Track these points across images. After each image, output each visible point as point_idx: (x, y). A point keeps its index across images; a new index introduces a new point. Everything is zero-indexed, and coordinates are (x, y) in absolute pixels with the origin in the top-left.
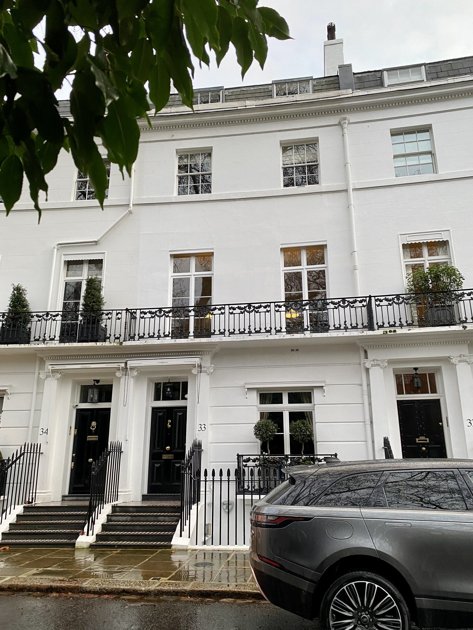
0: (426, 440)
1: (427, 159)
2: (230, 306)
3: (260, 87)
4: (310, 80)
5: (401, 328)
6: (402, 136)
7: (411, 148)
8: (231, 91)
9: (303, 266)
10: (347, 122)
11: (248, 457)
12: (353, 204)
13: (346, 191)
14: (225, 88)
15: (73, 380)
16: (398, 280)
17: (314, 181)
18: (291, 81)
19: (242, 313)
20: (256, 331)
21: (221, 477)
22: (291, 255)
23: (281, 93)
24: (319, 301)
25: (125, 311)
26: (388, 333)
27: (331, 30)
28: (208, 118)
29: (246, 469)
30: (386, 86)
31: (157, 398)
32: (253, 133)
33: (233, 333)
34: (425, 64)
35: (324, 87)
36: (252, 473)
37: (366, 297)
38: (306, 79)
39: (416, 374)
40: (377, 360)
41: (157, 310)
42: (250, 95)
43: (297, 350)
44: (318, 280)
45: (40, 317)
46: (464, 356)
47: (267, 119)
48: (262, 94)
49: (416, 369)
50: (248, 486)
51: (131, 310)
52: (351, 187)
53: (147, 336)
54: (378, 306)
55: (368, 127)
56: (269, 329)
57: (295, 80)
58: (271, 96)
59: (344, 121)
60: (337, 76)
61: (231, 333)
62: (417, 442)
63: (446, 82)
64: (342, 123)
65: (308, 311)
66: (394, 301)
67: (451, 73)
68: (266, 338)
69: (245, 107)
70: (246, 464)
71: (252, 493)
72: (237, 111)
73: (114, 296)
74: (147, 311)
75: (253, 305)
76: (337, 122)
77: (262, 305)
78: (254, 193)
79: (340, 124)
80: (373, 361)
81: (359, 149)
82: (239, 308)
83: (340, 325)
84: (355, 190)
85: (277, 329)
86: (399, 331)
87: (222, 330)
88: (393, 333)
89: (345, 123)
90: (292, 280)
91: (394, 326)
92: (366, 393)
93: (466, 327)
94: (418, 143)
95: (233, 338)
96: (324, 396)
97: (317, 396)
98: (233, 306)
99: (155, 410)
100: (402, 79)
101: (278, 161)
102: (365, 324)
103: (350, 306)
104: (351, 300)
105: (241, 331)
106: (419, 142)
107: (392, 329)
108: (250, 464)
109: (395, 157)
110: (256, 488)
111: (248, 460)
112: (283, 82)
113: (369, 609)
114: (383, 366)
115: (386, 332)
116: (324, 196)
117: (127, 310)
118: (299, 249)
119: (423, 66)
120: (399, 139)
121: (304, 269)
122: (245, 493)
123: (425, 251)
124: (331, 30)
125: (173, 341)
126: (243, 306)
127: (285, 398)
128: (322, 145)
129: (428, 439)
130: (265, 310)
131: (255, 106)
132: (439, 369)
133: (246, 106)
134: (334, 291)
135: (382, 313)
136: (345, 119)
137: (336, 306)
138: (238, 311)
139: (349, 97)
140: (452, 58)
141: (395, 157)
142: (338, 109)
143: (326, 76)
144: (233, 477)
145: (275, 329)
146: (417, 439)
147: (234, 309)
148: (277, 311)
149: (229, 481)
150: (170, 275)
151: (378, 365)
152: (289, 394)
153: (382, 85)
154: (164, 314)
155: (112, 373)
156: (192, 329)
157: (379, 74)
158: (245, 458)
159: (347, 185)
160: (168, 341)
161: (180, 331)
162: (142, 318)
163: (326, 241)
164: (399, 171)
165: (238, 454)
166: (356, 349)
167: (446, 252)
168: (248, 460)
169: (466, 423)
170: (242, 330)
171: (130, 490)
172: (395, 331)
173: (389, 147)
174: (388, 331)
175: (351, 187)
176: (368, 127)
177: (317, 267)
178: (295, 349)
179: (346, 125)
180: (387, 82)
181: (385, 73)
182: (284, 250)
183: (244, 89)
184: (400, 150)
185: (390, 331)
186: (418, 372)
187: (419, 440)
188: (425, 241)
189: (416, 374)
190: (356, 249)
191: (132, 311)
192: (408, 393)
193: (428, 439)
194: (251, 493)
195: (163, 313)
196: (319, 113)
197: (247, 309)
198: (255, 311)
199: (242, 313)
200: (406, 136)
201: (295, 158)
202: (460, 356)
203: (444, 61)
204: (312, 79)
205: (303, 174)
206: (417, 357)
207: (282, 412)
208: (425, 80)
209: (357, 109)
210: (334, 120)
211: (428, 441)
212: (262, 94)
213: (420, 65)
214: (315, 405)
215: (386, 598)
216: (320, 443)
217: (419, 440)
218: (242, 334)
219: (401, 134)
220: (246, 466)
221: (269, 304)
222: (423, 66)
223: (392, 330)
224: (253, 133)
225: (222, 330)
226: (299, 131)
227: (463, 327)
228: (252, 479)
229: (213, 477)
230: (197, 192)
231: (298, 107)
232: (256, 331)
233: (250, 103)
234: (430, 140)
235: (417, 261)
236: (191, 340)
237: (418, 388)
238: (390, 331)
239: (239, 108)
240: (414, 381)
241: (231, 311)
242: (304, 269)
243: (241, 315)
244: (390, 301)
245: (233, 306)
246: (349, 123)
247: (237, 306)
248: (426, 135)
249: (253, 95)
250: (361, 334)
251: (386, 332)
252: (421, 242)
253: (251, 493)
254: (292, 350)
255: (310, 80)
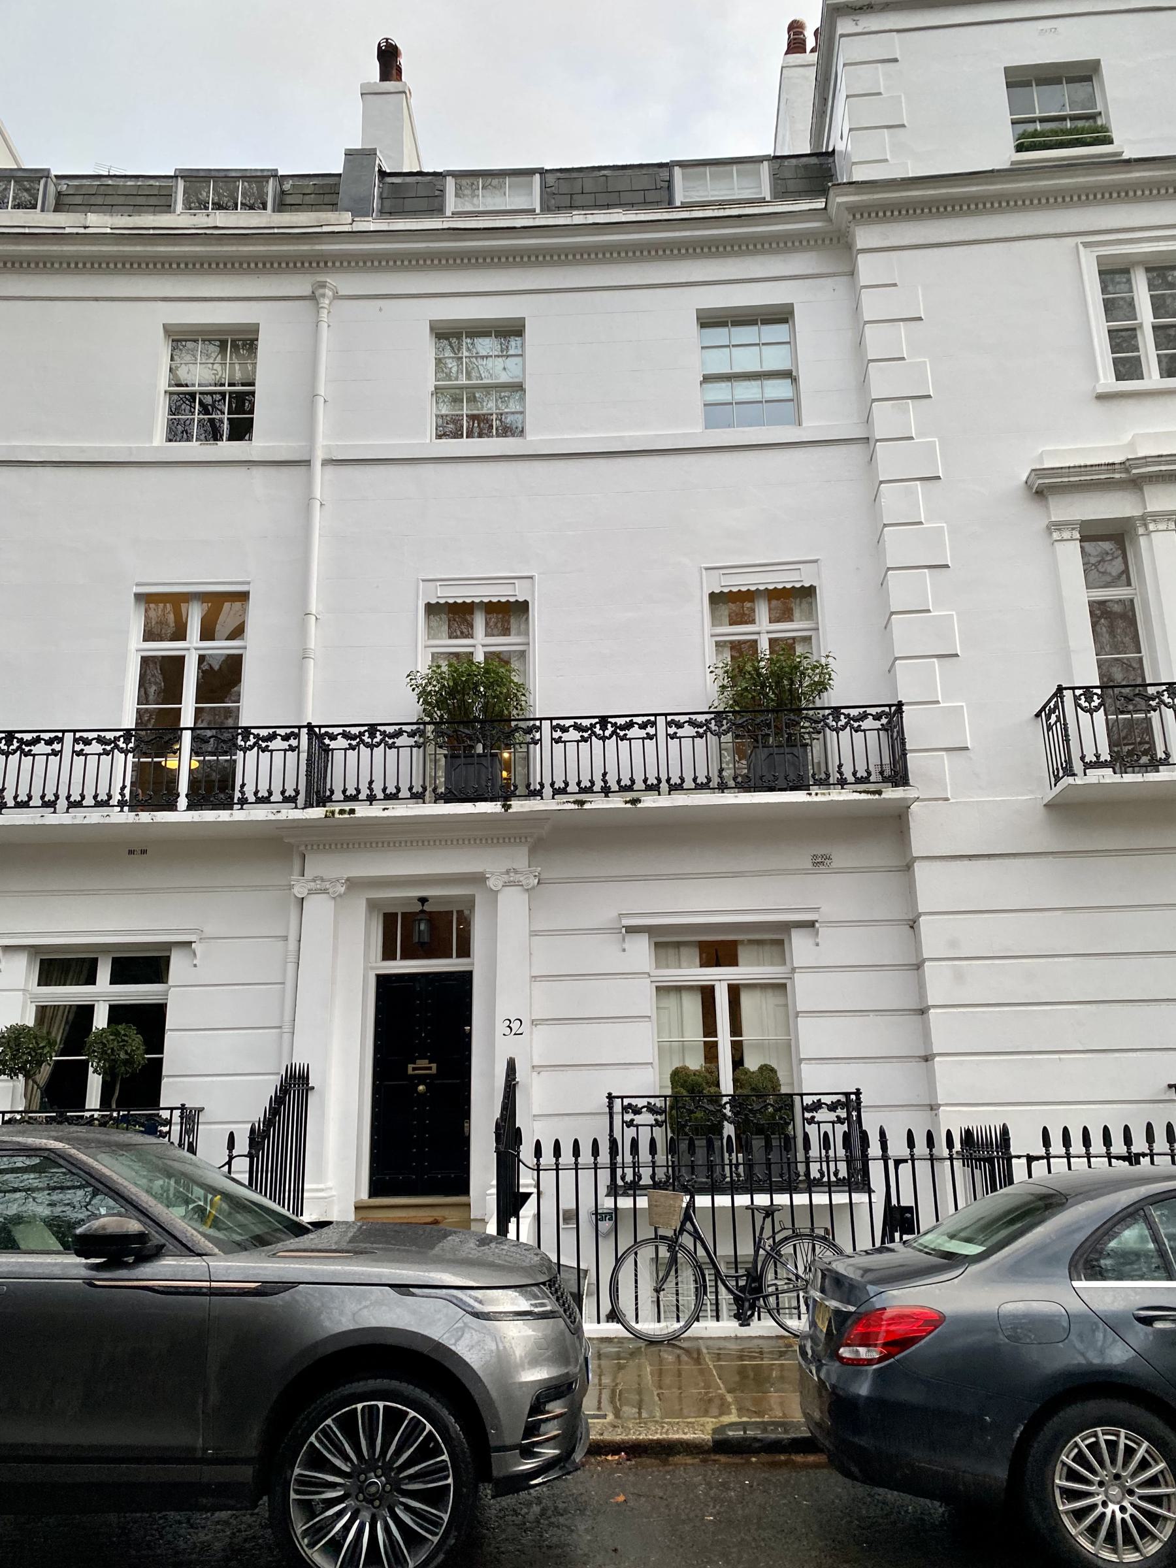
0: (430, 1068)
1: (779, 389)
2: (78, 735)
3: (152, 182)
4: (269, 177)
5: (607, 796)
6: (725, 330)
7: (746, 361)
8: (76, 182)
9: (190, 642)
10: (329, 293)
11: (815, 1098)
12: (318, 496)
13: (307, 463)
14: (53, 173)
15: (367, 899)
16: (691, 677)
17: (242, 430)
18: (222, 174)
19: (354, 749)
20: (647, 786)
21: (557, 1160)
22: (164, 612)
23: (195, 203)
24: (223, 736)
25: (305, 730)
26: (337, 816)
27: (388, 57)
28: (26, 248)
29: (812, 1130)
30: (448, 214)
31: (388, 954)
32: (96, 299)
33: (78, 804)
34: (542, 172)
35: (308, 199)
36: (826, 1142)
37: (299, 727)
38: (259, 174)
39: (422, 911)
40: (322, 880)
41: (118, 734)
42: (121, 200)
43: (144, 852)
44: (223, 679)
45: (353, 738)
46: (516, 871)
47: (135, 266)
48: (153, 201)
49: (423, 900)
50: (821, 1171)
51: (320, 727)
52: (319, 455)
53: (88, 801)
54: (78, 755)
55: (381, 310)
56: (293, 794)
57: (234, 174)
58: (168, 208)
59: (321, 291)
60: (340, 175)
61: (73, 805)
62: (410, 1072)
63: (568, 221)
64: (317, 294)
65: (130, 755)
66: (708, 728)
67: (602, 199)
68: (38, 821)
69: (82, 231)
70: (813, 1117)
71: (830, 1188)
72: (58, 237)
73: (553, 686)
74: (336, 731)
75: (613, 720)
76: (307, 291)
77: (635, 720)
78: (82, 450)
79: (313, 297)
80: (314, 880)
81: (354, 360)
82: (577, 727)
83: (592, 782)
84: (326, 462)
85: (556, 786)
86: (363, 811)
87: (652, 781)
88: (346, 816)
89: (323, 295)
90: (161, 676)
91: (354, 798)
92: (292, 958)
93: (510, 806)
94: (749, 351)
95: (77, 817)
96: (195, 966)
97: (178, 965)
98: (676, 718)
99: (385, 983)
100: (489, 200)
101: (151, 375)
102: (887, 773)
103: (260, 747)
104: (854, 712)
105: (348, 793)
106: (733, 349)
107: (347, 807)
108: (822, 1115)
109: (707, 379)
110: (840, 1176)
111: (817, 1106)
112: (202, 174)
113: (392, 1469)
114: (528, 884)
115: (333, 812)
116: (257, 472)
117: (310, 727)
118: (188, 597)
119: (766, 163)
120: (719, 335)
121: (192, 648)
122: (638, 1192)
123: (479, 622)
124: (388, 57)
125: (127, 817)
126: (586, 723)
127: (104, 972)
128: (1011, 144)
129: (434, 1066)
130: (643, 733)
131: (109, 231)
132: (471, 902)
133: (85, 227)
134: (255, 706)
135: (348, 768)
136: (323, 285)
137: (586, 735)
138: (574, 735)
139: (333, 232)
140: (558, 167)
141: (707, 379)
142: (307, 259)
143: (778, 154)
144: (604, 1157)
145: (68, 797)
146: (410, 1066)
147: (565, 730)
148: (673, 736)
149: (596, 1169)
150: (136, 647)
151: (325, 891)
152: (115, 961)
153: (437, 209)
154: (19, 748)
155: (479, 879)
156: (183, 787)
157: (664, 174)
158: (808, 1100)
159: (312, 448)
160: (120, 817)
161: (153, 790)
162: (80, 753)
163: (248, 583)
164: (714, 413)
165: (610, 1094)
166: (279, 848)
167: (811, 614)
168: (817, 1106)
169: (501, 1028)
170: (351, 791)
171: (330, 1184)
172: (352, 811)
173: (692, 353)
174: (337, 809)
175: (319, 455)
176: (381, 310)
177: (165, 648)
178: (135, 851)
179: (327, 302)
180: (451, 203)
181: (450, 183)
182: (144, 599)
183: (110, 182)
184: (719, 363)
185: (342, 812)
186: (427, 908)
187: (414, 1069)
188: (762, 588)
189: (422, 911)
190: (313, 608)
191: (323, 730)
192: (404, 957)
193: (434, 1066)
194: (826, 1189)
195: (252, 740)
196: (264, 265)
197: (366, 738)
198: (852, 727)
199: (584, 740)
200: (734, 330)
201: (202, 373)
202: (508, 872)
203: (641, 166)
204: (274, 174)
205: (227, 415)
206: (417, 871)
207: (713, 986)
208: (538, 211)
209: (357, 263)
210: (299, 285)
211: (434, 1071)
212: (153, 201)
213: (530, 172)
214: (793, 970)
215: (317, 1445)
216: (171, 1080)
217: (414, 1069)
218: (102, 806)
219: (723, 324)
220: (811, 1121)
221: (652, 718)
222: (538, 176)
223: (347, 808)
224: (96, 299)
225: (652, 781)
226: (217, 304)
227: (503, 806)
228: (731, 1160)
229: (557, 1160)
230: (457, 434)
231: (210, 245)
232: (647, 786)
233: (98, 222)
234: (789, 343)
235: (741, 632)
236: (182, 815)
237: (422, 944)
238: (342, 812)
239: (68, 231)
240: (427, 928)
241: (671, 731)
242: (192, 648)
243: (697, 740)
244: (354, 739)
245: (562, 722)
246: (337, 297)
247: (571, 722)
248: (778, 332)
249: (132, 201)
250: (273, 817)
251: (333, 812)
252: (753, 588)
253: (826, 1189)
254: (131, 852)
255: (269, 177)
